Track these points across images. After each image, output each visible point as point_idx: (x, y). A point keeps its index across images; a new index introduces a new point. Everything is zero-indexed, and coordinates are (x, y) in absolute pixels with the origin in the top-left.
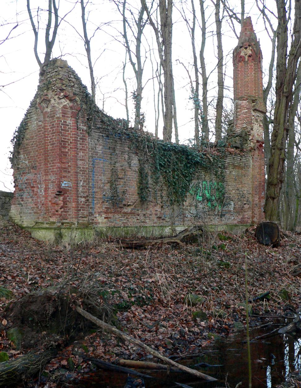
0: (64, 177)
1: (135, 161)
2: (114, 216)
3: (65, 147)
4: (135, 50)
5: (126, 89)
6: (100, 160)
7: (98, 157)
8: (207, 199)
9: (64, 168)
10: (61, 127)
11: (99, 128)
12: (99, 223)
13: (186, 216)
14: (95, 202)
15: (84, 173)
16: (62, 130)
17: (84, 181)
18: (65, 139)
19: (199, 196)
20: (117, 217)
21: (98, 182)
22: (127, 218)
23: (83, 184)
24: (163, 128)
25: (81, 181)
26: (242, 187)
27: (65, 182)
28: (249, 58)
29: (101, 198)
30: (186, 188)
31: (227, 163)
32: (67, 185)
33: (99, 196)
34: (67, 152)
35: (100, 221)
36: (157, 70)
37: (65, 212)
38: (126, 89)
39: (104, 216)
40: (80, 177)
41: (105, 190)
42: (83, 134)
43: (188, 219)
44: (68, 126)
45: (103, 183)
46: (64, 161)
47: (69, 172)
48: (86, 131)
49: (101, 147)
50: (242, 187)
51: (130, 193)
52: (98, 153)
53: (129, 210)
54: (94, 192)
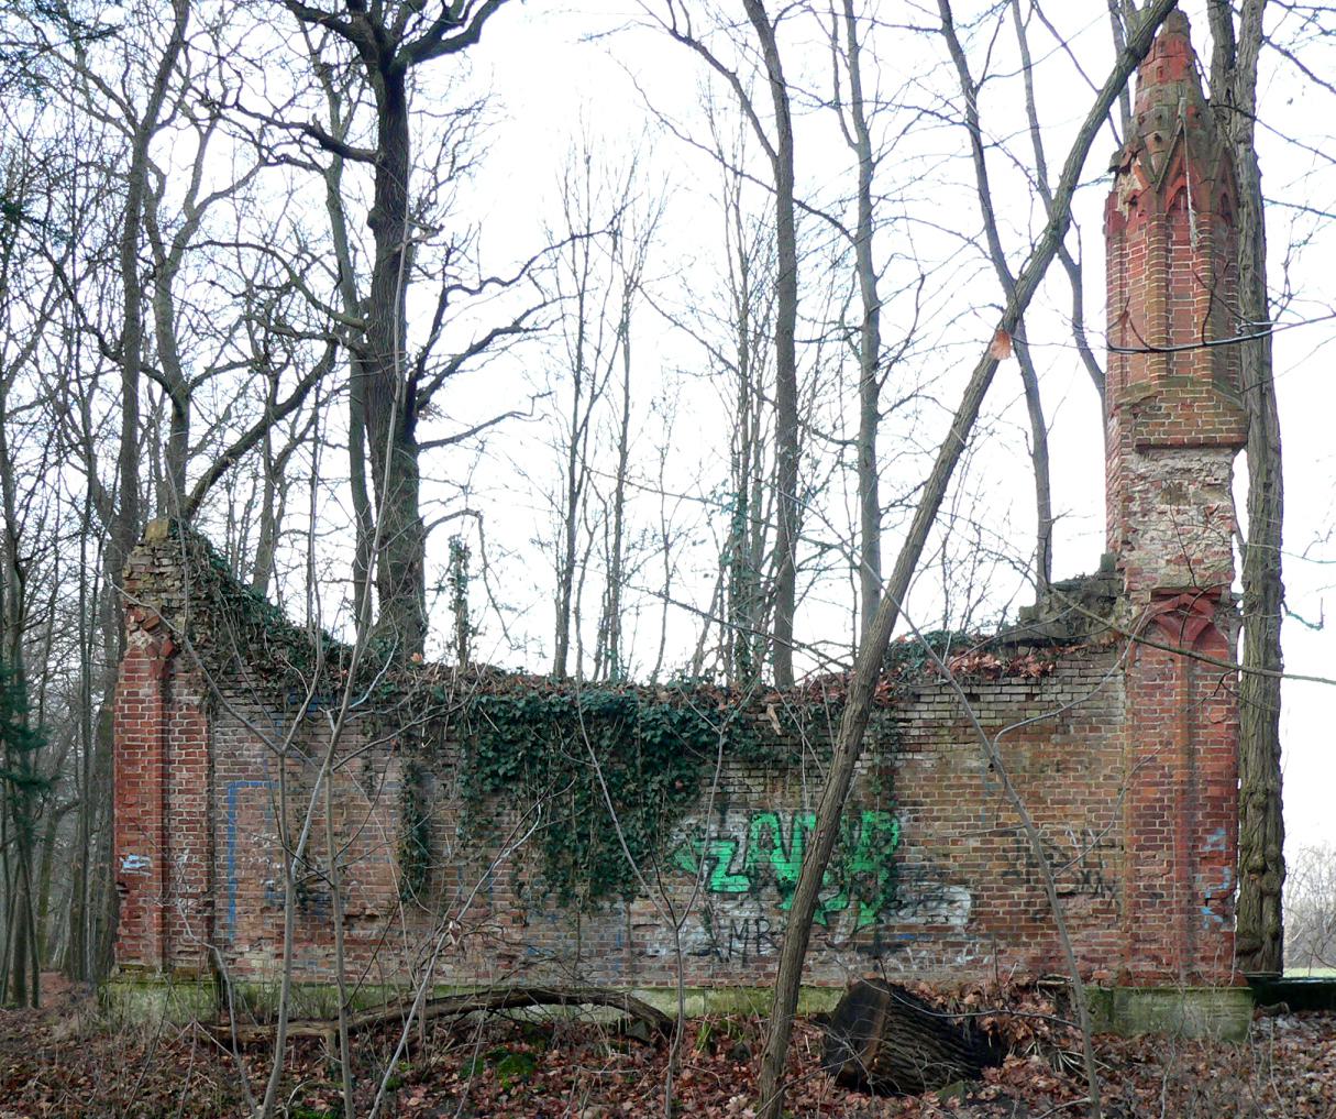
0: (129, 844)
1: (392, 775)
2: (306, 951)
3: (133, 763)
4: (772, 175)
5: (457, 514)
6: (255, 786)
7: (247, 778)
8: (777, 883)
9: (131, 820)
10: (122, 709)
11: (248, 691)
12: (252, 971)
13: (650, 951)
14: (239, 909)
15: (194, 829)
16: (124, 716)
17: (192, 851)
18: (134, 739)
19: (728, 874)
20: (320, 952)
21: (247, 851)
22: (357, 957)
23: (189, 859)
24: (1283, 649)
25: (182, 850)
26: (1037, 818)
27: (131, 858)
28: (1122, 178)
29: (256, 898)
30: (649, 849)
31: (915, 723)
32: (138, 865)
33: (251, 891)
34: (139, 776)
35: (255, 964)
36: (594, 398)
37: (134, 938)
38: (457, 514)
39: (270, 949)
40: (180, 839)
41: (275, 871)
42: (191, 716)
43: (657, 965)
44: (143, 702)
45: (268, 853)
46: (131, 799)
47: (145, 828)
48: (199, 706)
49: (259, 745)
50: (1037, 818)
51: (373, 879)
52: (249, 763)
53: (373, 931)
54: (235, 881)
